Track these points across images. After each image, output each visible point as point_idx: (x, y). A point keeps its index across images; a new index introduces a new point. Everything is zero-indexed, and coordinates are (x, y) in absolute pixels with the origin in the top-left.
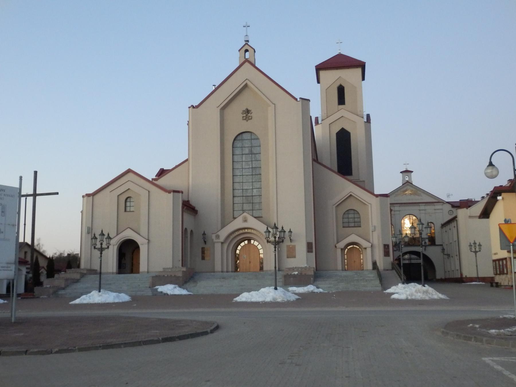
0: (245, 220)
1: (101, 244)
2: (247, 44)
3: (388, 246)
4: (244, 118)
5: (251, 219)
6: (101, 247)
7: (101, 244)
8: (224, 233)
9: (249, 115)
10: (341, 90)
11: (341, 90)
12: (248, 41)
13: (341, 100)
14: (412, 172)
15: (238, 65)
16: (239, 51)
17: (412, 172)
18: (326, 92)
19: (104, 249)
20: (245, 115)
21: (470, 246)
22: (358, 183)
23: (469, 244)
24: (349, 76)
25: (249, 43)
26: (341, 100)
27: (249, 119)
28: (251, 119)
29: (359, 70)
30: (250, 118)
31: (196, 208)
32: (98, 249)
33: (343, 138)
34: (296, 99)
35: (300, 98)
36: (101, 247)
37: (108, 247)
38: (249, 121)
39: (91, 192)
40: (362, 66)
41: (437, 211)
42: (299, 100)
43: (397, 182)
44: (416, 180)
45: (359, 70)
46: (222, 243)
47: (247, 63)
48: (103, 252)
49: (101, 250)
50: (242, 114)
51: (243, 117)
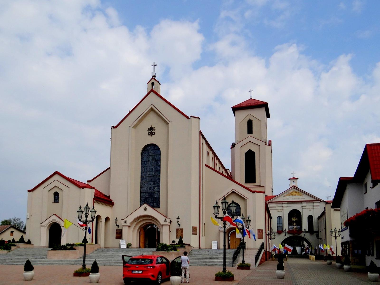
0: (145, 209)
1: (86, 217)
2: (154, 79)
3: (262, 230)
4: (149, 134)
5: (149, 208)
6: (336, 235)
7: (86, 217)
8: (129, 220)
9: (153, 131)
10: (250, 123)
11: (250, 123)
12: (155, 76)
13: (250, 131)
14: (298, 179)
15: (146, 94)
16: (147, 83)
17: (298, 179)
18: (238, 124)
19: (337, 236)
20: (150, 131)
21: (80, 211)
22: (250, 188)
23: (78, 209)
24: (258, 114)
25: (155, 78)
26: (250, 131)
27: (153, 134)
28: (154, 134)
29: (263, 110)
30: (153, 133)
31: (113, 201)
32: (334, 236)
33: (250, 158)
34: (188, 118)
35: (191, 116)
36: (336, 235)
37: (339, 236)
38: (153, 136)
39: (31, 189)
40: (265, 106)
41: (315, 207)
42: (190, 117)
43: (287, 185)
44: (300, 184)
45: (263, 110)
46: (129, 227)
47: (152, 93)
48: (337, 238)
49: (336, 237)
50: (148, 130)
51: (148, 133)
